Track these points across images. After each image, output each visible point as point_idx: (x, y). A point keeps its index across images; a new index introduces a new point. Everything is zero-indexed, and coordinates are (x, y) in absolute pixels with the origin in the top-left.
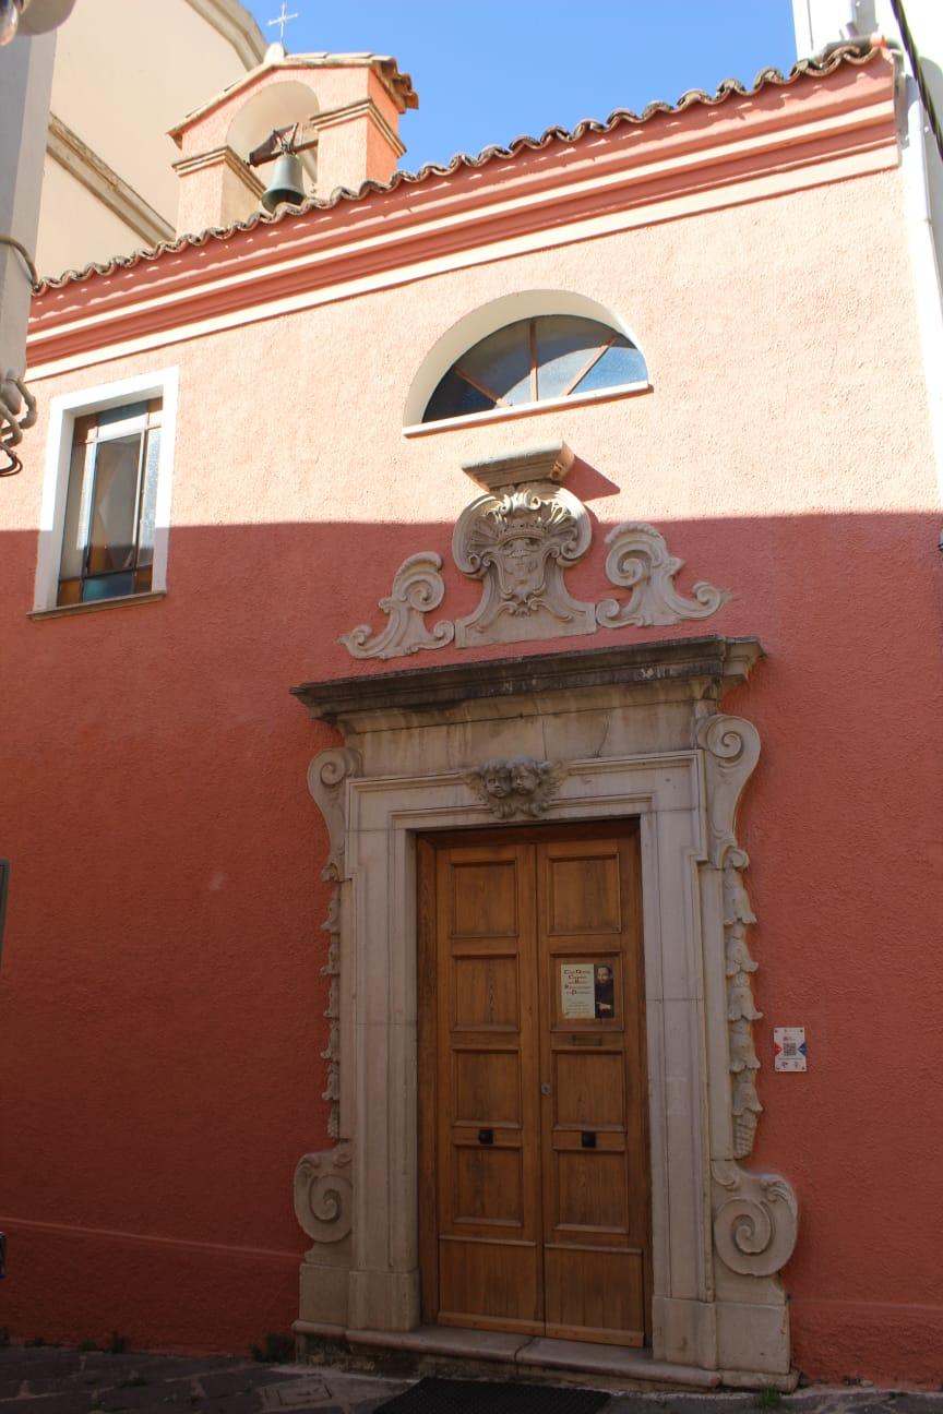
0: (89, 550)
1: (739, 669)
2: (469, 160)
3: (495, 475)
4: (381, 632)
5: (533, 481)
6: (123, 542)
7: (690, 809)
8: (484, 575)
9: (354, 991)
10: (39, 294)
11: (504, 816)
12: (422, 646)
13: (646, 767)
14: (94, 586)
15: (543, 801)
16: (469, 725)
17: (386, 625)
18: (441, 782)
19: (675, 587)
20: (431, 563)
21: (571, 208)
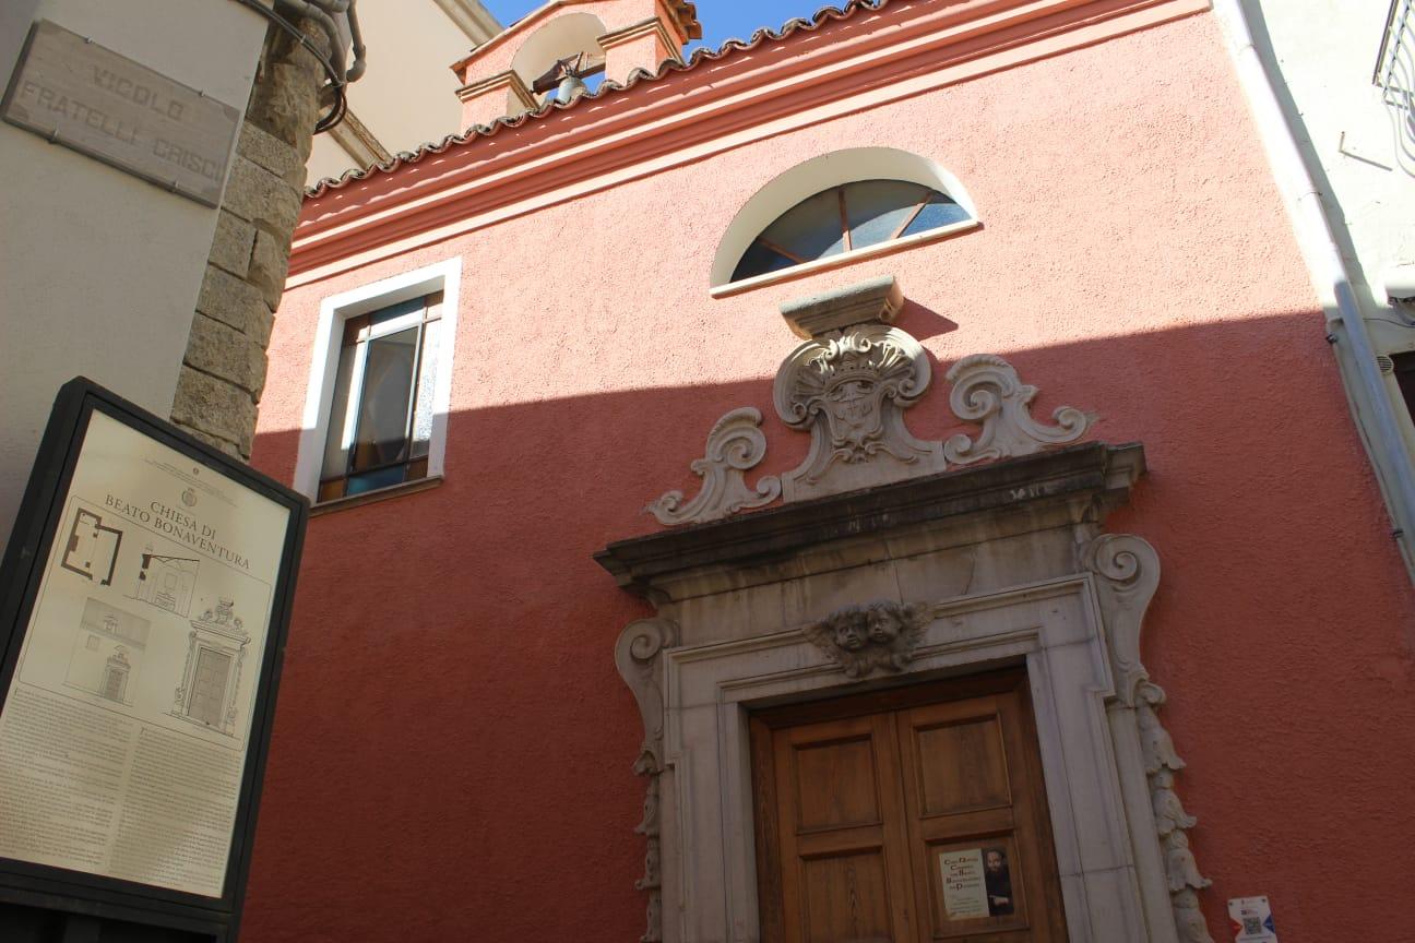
0: (355, 447)
1: (1122, 481)
2: (772, 34)
3: (814, 319)
4: (695, 496)
5: (860, 323)
6: (394, 436)
7: (1087, 641)
8: (812, 425)
10: (317, 196)
11: (859, 674)
12: (744, 505)
13: (1028, 598)
14: (357, 484)
15: (906, 650)
16: (807, 580)
17: (700, 489)
18: (781, 641)
19: (1032, 416)
20: (748, 418)
21: (880, 73)
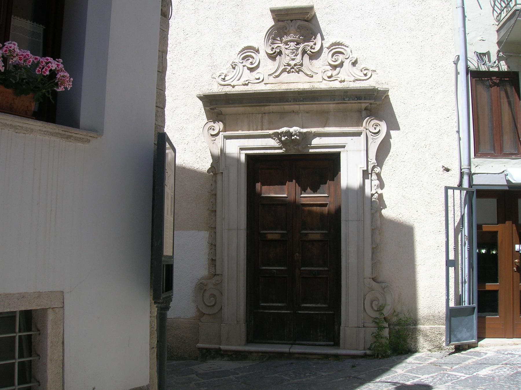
9: (224, 217)
12: (249, 81)
